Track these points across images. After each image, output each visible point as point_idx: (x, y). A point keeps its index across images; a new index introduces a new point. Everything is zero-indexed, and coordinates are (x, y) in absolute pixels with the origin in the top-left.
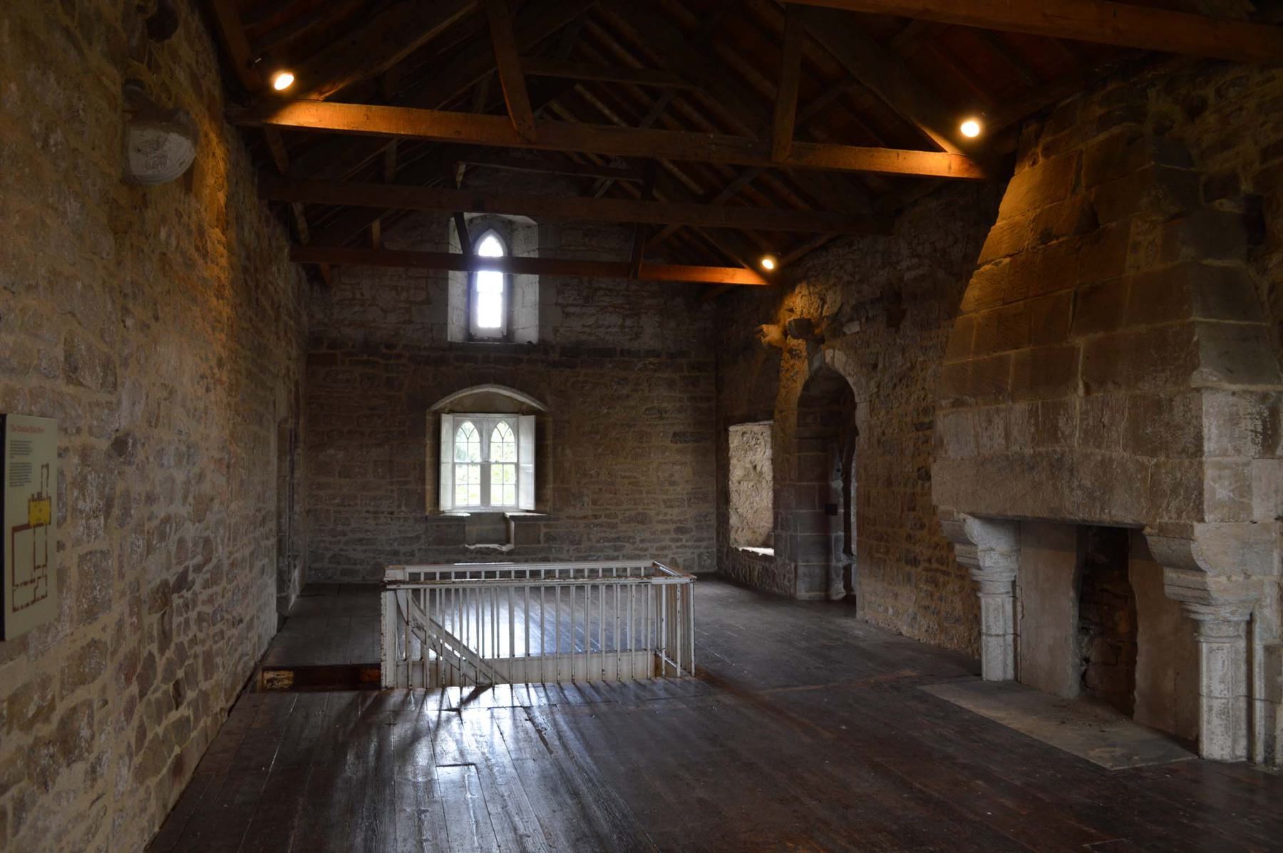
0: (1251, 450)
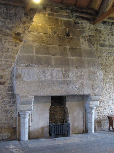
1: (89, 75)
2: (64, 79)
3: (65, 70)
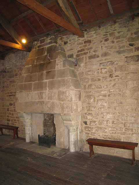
0: (78, 100)
1: (59, 95)
2: (39, 100)
3: (40, 92)
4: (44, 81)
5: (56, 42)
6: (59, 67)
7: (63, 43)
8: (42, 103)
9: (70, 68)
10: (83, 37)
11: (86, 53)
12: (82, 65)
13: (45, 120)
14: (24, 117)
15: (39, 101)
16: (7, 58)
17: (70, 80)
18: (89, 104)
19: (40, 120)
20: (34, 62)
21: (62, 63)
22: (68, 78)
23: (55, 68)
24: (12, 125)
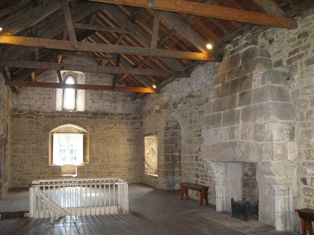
0: (287, 139)
1: (255, 132)
4: (236, 109)
5: (255, 43)
6: (256, 85)
7: (267, 42)
8: (234, 144)
9: (274, 85)
10: (296, 26)
11: (301, 55)
12: (296, 77)
13: (246, 174)
14: (213, 169)
15: (230, 142)
16: (193, 75)
17: (269, 105)
18: (309, 146)
19: (237, 173)
20: (224, 79)
21: (260, 77)
22: (269, 102)
23: (251, 87)
24: (202, 184)
